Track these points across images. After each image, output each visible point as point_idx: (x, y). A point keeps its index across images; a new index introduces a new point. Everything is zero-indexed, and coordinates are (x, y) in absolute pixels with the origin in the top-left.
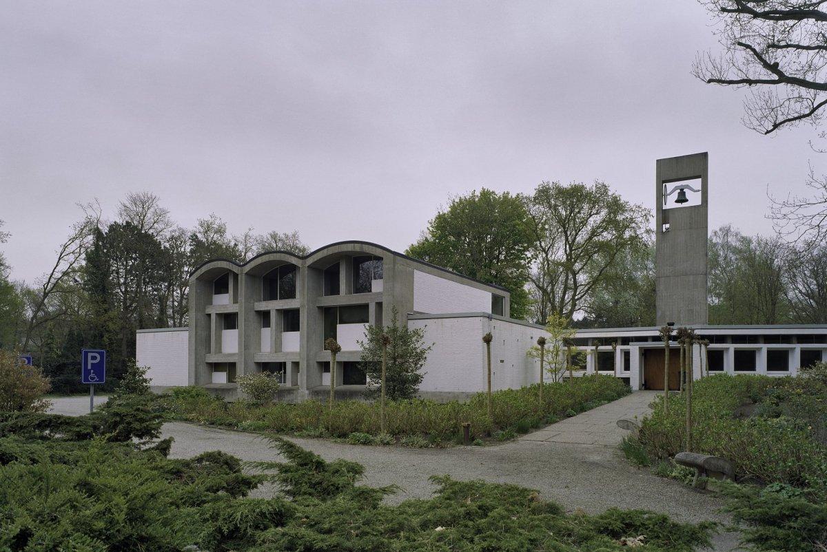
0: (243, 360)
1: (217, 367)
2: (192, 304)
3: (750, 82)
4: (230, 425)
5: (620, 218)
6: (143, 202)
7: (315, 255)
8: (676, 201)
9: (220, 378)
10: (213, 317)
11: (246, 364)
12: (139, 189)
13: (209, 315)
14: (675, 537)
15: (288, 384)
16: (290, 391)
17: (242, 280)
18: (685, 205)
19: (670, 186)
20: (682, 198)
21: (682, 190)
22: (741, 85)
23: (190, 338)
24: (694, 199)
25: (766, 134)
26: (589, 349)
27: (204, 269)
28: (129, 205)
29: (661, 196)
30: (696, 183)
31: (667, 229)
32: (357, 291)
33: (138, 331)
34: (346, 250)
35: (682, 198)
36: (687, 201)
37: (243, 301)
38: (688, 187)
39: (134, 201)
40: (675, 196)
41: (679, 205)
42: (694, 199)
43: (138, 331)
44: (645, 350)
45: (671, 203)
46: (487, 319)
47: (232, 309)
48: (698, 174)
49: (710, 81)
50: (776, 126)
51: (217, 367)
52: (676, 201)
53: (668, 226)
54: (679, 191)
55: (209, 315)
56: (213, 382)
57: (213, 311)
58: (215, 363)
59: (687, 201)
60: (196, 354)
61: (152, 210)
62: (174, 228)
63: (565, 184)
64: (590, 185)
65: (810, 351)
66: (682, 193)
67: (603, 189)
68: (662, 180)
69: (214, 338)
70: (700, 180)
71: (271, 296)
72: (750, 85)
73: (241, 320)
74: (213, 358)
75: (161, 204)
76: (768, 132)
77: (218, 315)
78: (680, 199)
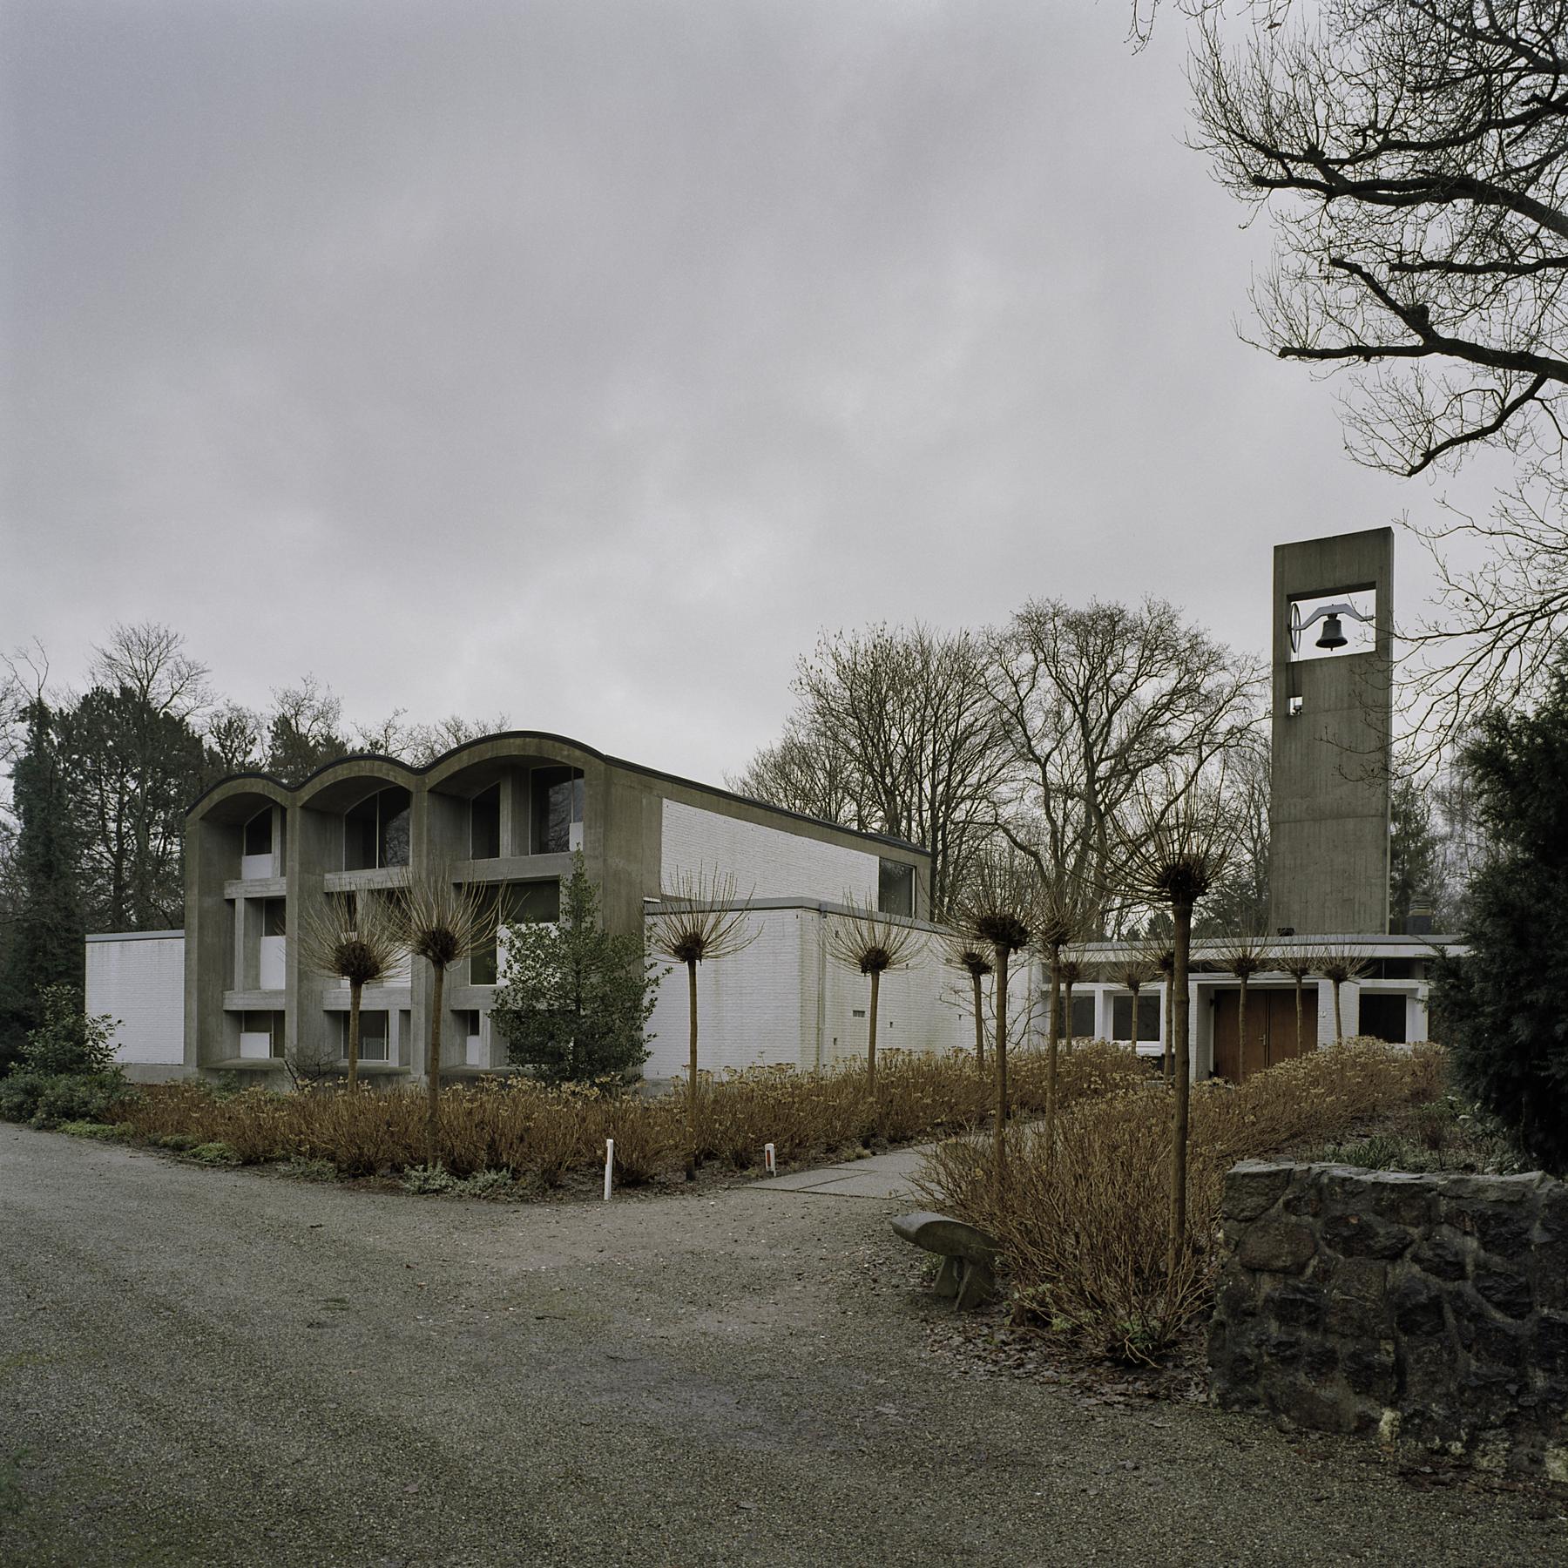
0: (295, 1003)
1: (251, 1020)
2: (194, 874)
3: (1366, 353)
4: (179, 1148)
5: (1208, 684)
6: (151, 648)
7: (443, 766)
8: (1320, 644)
9: (256, 1047)
10: (240, 906)
11: (302, 1012)
12: (138, 616)
13: (232, 902)
14: (351, 1366)
15: (393, 1062)
16: (390, 1076)
17: (295, 818)
18: (1339, 651)
19: (1307, 607)
20: (1332, 638)
21: (1333, 616)
22: (1344, 360)
23: (187, 952)
24: (1359, 638)
25: (1410, 474)
26: (1098, 989)
27: (217, 796)
28: (116, 655)
29: (1284, 633)
30: (1365, 601)
31: (1298, 709)
32: (541, 847)
33: (88, 937)
34: (504, 753)
35: (1332, 638)
36: (1343, 642)
37: (297, 868)
38: (1345, 609)
39: (126, 645)
40: (1317, 631)
41: (1326, 653)
42: (1359, 638)
43: (88, 937)
44: (1217, 992)
45: (1307, 648)
46: (815, 915)
47: (277, 889)
48: (1366, 580)
49: (1285, 353)
50: (1429, 456)
51: (251, 1020)
52: (1320, 644)
53: (1299, 701)
54: (1325, 618)
55: (232, 902)
56: (242, 1056)
57: (237, 891)
58: (246, 1011)
59: (1343, 642)
60: (201, 991)
61: (170, 664)
62: (219, 705)
63: (1079, 603)
64: (1135, 609)
65: (1265, 991)
66: (1333, 624)
67: (1166, 620)
68: (1286, 598)
69: (242, 957)
70: (1371, 595)
71: (364, 857)
72: (1367, 359)
73: (292, 912)
74: (238, 1000)
75: (189, 650)
76: (1414, 471)
77: (250, 901)
78: (1330, 636)
